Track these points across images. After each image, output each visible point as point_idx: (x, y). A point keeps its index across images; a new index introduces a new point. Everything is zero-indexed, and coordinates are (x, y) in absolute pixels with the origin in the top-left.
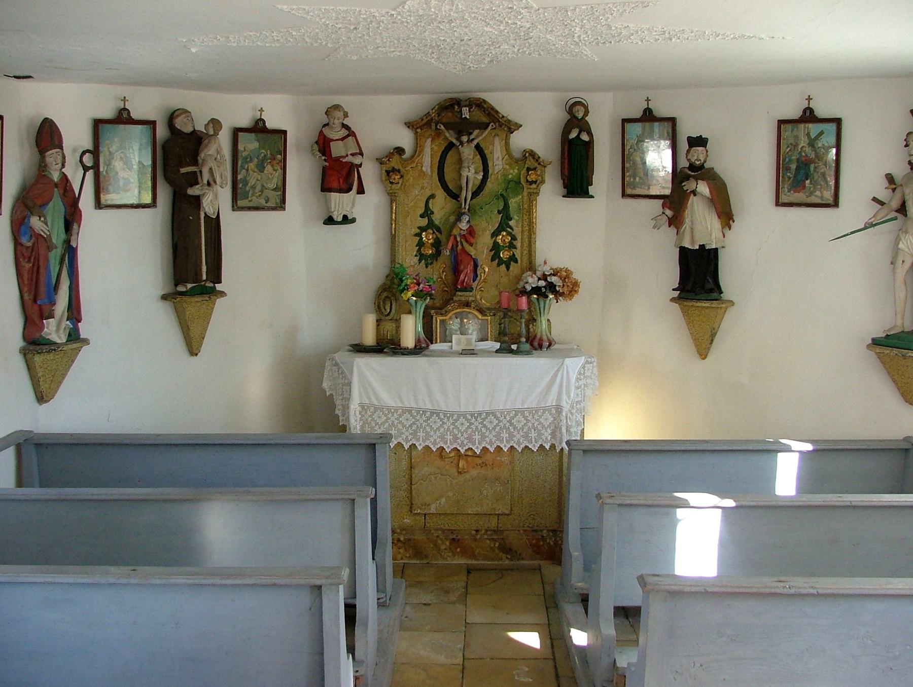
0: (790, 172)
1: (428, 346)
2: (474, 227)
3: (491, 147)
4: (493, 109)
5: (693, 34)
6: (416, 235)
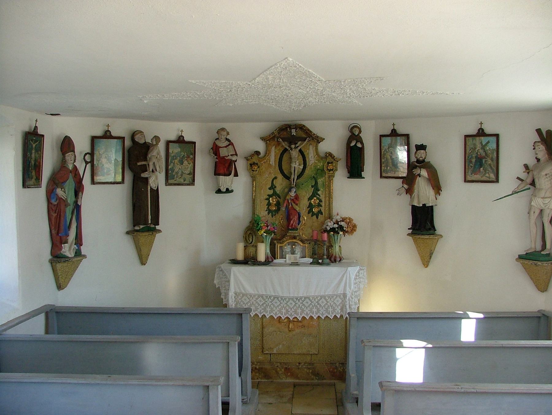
0: (472, 164)
1: (273, 261)
2: (298, 194)
3: (308, 151)
4: (309, 130)
5: (410, 92)
6: (266, 199)
